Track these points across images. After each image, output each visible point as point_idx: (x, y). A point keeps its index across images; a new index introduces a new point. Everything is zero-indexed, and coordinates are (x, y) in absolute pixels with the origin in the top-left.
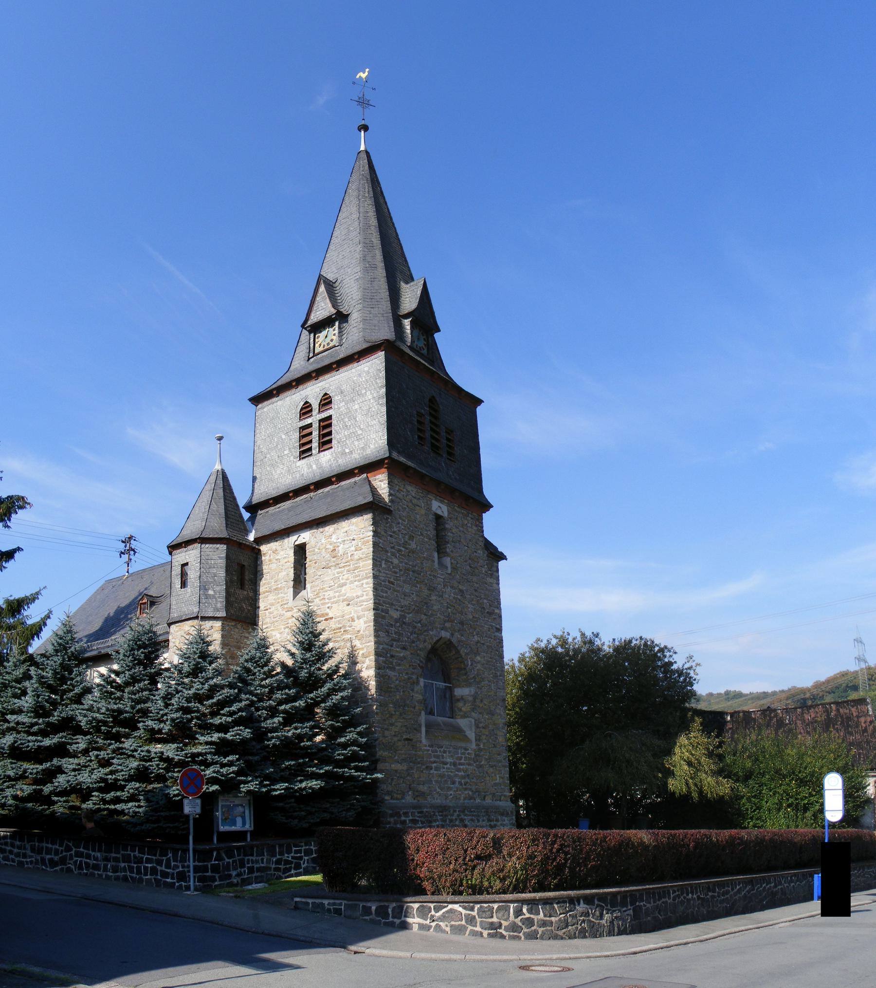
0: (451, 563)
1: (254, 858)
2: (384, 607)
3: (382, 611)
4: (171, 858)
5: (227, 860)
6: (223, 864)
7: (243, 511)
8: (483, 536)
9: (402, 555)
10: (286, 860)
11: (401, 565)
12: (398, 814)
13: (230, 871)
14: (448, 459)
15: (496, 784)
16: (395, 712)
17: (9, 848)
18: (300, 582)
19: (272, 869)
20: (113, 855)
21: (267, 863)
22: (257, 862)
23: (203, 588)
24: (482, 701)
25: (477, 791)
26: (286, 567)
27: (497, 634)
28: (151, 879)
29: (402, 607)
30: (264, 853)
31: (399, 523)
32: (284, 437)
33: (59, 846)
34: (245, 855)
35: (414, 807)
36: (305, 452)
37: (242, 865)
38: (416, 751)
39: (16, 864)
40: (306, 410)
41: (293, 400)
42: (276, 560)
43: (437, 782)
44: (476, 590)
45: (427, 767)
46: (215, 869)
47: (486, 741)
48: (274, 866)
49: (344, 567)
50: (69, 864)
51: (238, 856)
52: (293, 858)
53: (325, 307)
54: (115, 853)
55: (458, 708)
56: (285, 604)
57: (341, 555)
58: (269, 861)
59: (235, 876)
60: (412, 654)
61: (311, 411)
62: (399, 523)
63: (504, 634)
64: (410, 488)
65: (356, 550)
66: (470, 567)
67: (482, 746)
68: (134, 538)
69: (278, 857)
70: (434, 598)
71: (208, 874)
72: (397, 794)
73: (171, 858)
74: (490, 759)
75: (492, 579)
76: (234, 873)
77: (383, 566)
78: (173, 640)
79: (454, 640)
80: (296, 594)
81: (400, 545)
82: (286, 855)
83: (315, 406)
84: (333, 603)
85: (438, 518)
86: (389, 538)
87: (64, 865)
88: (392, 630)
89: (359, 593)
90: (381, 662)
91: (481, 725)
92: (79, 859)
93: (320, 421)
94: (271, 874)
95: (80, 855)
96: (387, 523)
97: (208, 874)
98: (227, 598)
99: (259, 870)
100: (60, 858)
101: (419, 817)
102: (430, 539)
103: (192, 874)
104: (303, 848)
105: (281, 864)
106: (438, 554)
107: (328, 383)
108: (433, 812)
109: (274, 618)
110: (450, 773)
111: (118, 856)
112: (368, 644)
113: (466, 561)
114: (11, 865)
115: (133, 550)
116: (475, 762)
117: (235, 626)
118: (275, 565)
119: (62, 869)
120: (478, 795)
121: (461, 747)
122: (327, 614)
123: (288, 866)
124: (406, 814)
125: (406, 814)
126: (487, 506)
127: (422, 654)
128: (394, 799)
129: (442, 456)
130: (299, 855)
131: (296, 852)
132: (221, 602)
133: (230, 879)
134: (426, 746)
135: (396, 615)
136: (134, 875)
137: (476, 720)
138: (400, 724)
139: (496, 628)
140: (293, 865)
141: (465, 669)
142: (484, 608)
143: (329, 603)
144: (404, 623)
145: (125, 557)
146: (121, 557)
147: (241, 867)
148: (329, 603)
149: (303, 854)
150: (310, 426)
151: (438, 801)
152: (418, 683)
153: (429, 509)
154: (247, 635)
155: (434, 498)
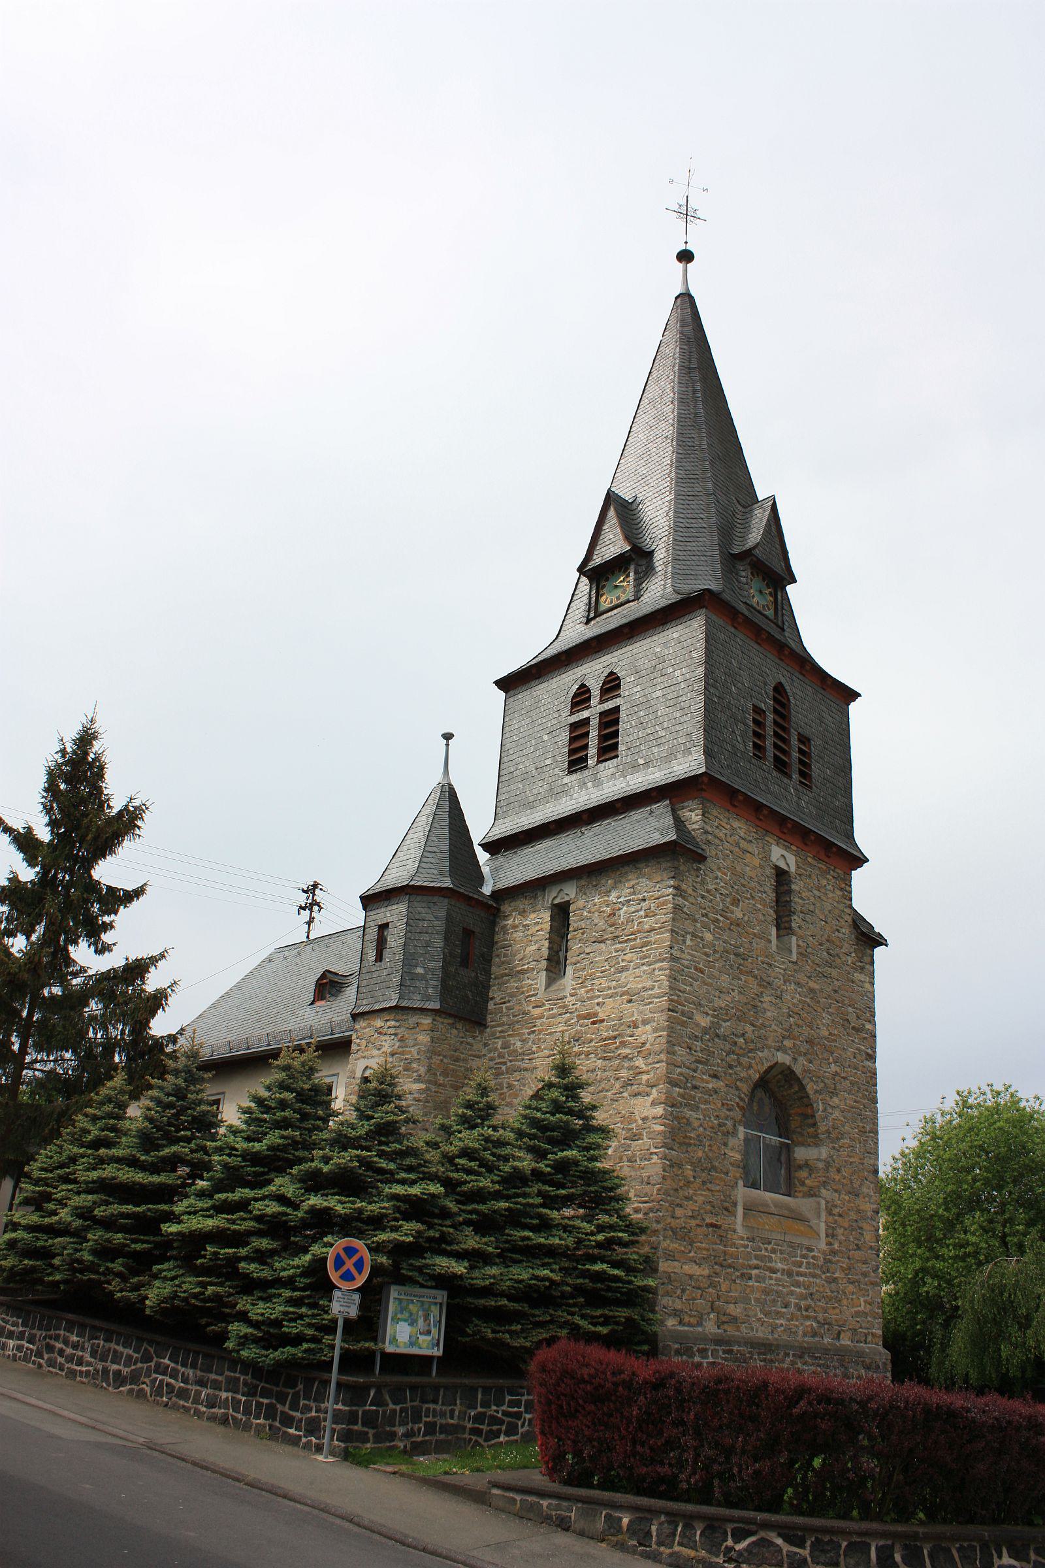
0: (798, 946)
1: (438, 1408)
2: (686, 1008)
3: (683, 1014)
4: (302, 1393)
5: (391, 1406)
6: (384, 1412)
7: (479, 851)
8: (851, 906)
9: (719, 928)
10: (492, 1417)
11: (717, 943)
12: (689, 1352)
13: (394, 1426)
14: (800, 782)
15: (857, 1314)
16: (694, 1177)
17: (59, 1345)
18: (558, 962)
19: (467, 1430)
20: (213, 1376)
21: (459, 1417)
22: (443, 1414)
23: (409, 960)
24: (839, 1171)
25: (826, 1323)
26: (537, 938)
27: (868, 1063)
28: (264, 1426)
29: (715, 1011)
30: (456, 1400)
31: (717, 878)
32: (545, 738)
33: (134, 1351)
34: (423, 1401)
35: (718, 1341)
36: (576, 763)
37: (417, 1418)
38: (725, 1246)
39: (64, 1374)
40: (581, 698)
41: (566, 682)
42: (524, 926)
43: (757, 1300)
44: (836, 991)
45: (743, 1275)
46: (370, 1419)
47: (843, 1238)
48: (470, 1425)
49: (626, 941)
50: (143, 1383)
51: (411, 1401)
52: (505, 1413)
53: (614, 540)
54: (217, 1374)
55: (799, 1180)
56: (532, 995)
57: (623, 923)
58: (463, 1415)
59: (403, 1435)
60: (727, 1085)
61: (589, 699)
62: (717, 878)
63: (878, 1065)
64: (736, 824)
65: (646, 916)
66: (829, 954)
67: (836, 1246)
68: (320, 887)
69: (480, 1409)
70: (766, 999)
71: (356, 1427)
72: (691, 1316)
73: (302, 1393)
74: (849, 1269)
75: (863, 976)
76: (401, 1430)
77: (688, 942)
78: (358, 1041)
79: (798, 1069)
80: (550, 982)
81: (717, 913)
82: (494, 1408)
83: (596, 692)
84: (606, 997)
85: (781, 875)
86: (699, 899)
87: (135, 1384)
88: (696, 1046)
89: (648, 984)
90: (675, 1095)
91: (836, 1211)
92: (160, 1377)
93: (601, 714)
94: (465, 1439)
95: (160, 1369)
96: (698, 877)
97: (356, 1427)
98: (443, 981)
99: (445, 1429)
100: (132, 1371)
101: (725, 1359)
102: (764, 906)
103: (328, 1424)
104: (524, 1398)
105: (483, 1423)
106: (778, 930)
107: (616, 660)
108: (749, 1353)
109: (514, 1016)
110: (781, 1288)
111: (220, 1378)
112: (657, 1065)
113: (821, 944)
114: (57, 1374)
115: (318, 904)
116: (824, 1273)
117: (452, 1025)
118: (521, 934)
119: (131, 1391)
120: (828, 1330)
121: (800, 1246)
122: (596, 1015)
123: (495, 1428)
124: (703, 1352)
125: (703, 1352)
126: (859, 860)
127: (745, 1088)
128: (684, 1325)
129: (790, 777)
130: (516, 1409)
131: (512, 1404)
132: (435, 987)
133: (394, 1441)
134: (742, 1238)
135: (704, 1021)
136: (239, 1416)
137: (827, 1202)
138: (703, 1198)
139: (867, 1054)
140: (504, 1428)
141: (813, 1116)
142: (848, 1020)
143: (599, 996)
144: (718, 1036)
145: (306, 914)
146: (299, 914)
147: (414, 1422)
148: (599, 996)
149: (522, 1409)
150: (586, 721)
151: (761, 1333)
152: (734, 1133)
153: (767, 857)
154: (470, 1040)
155: (775, 843)
